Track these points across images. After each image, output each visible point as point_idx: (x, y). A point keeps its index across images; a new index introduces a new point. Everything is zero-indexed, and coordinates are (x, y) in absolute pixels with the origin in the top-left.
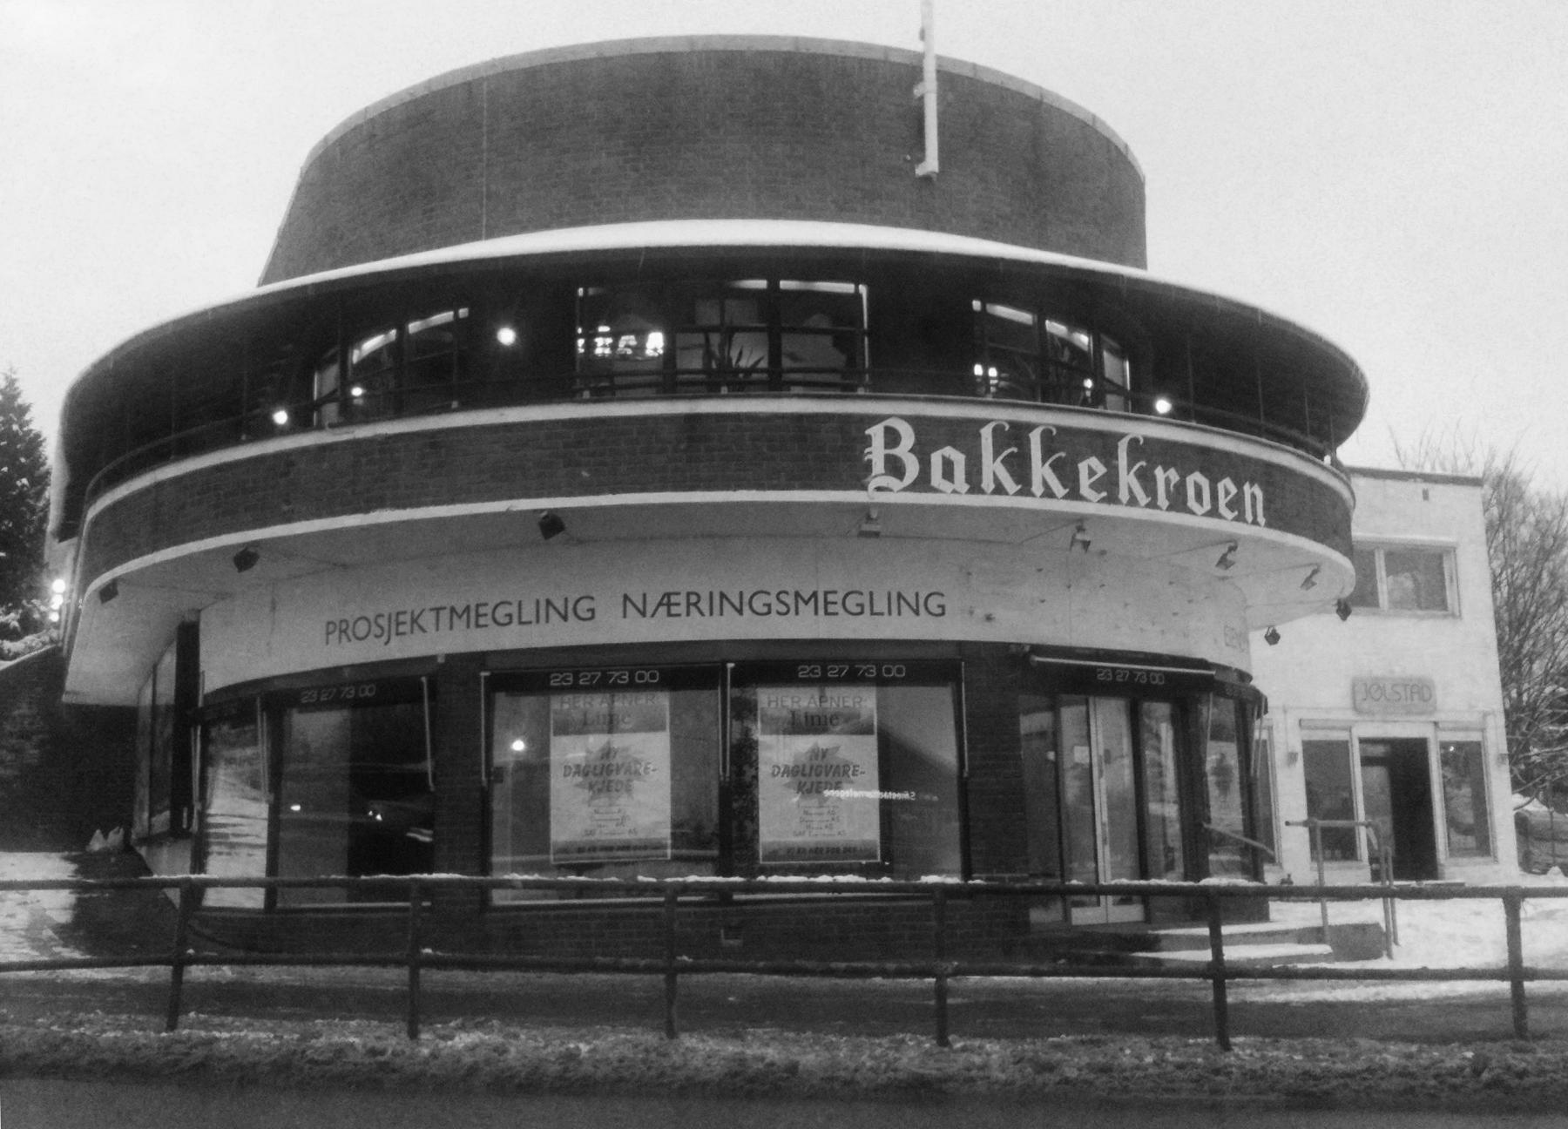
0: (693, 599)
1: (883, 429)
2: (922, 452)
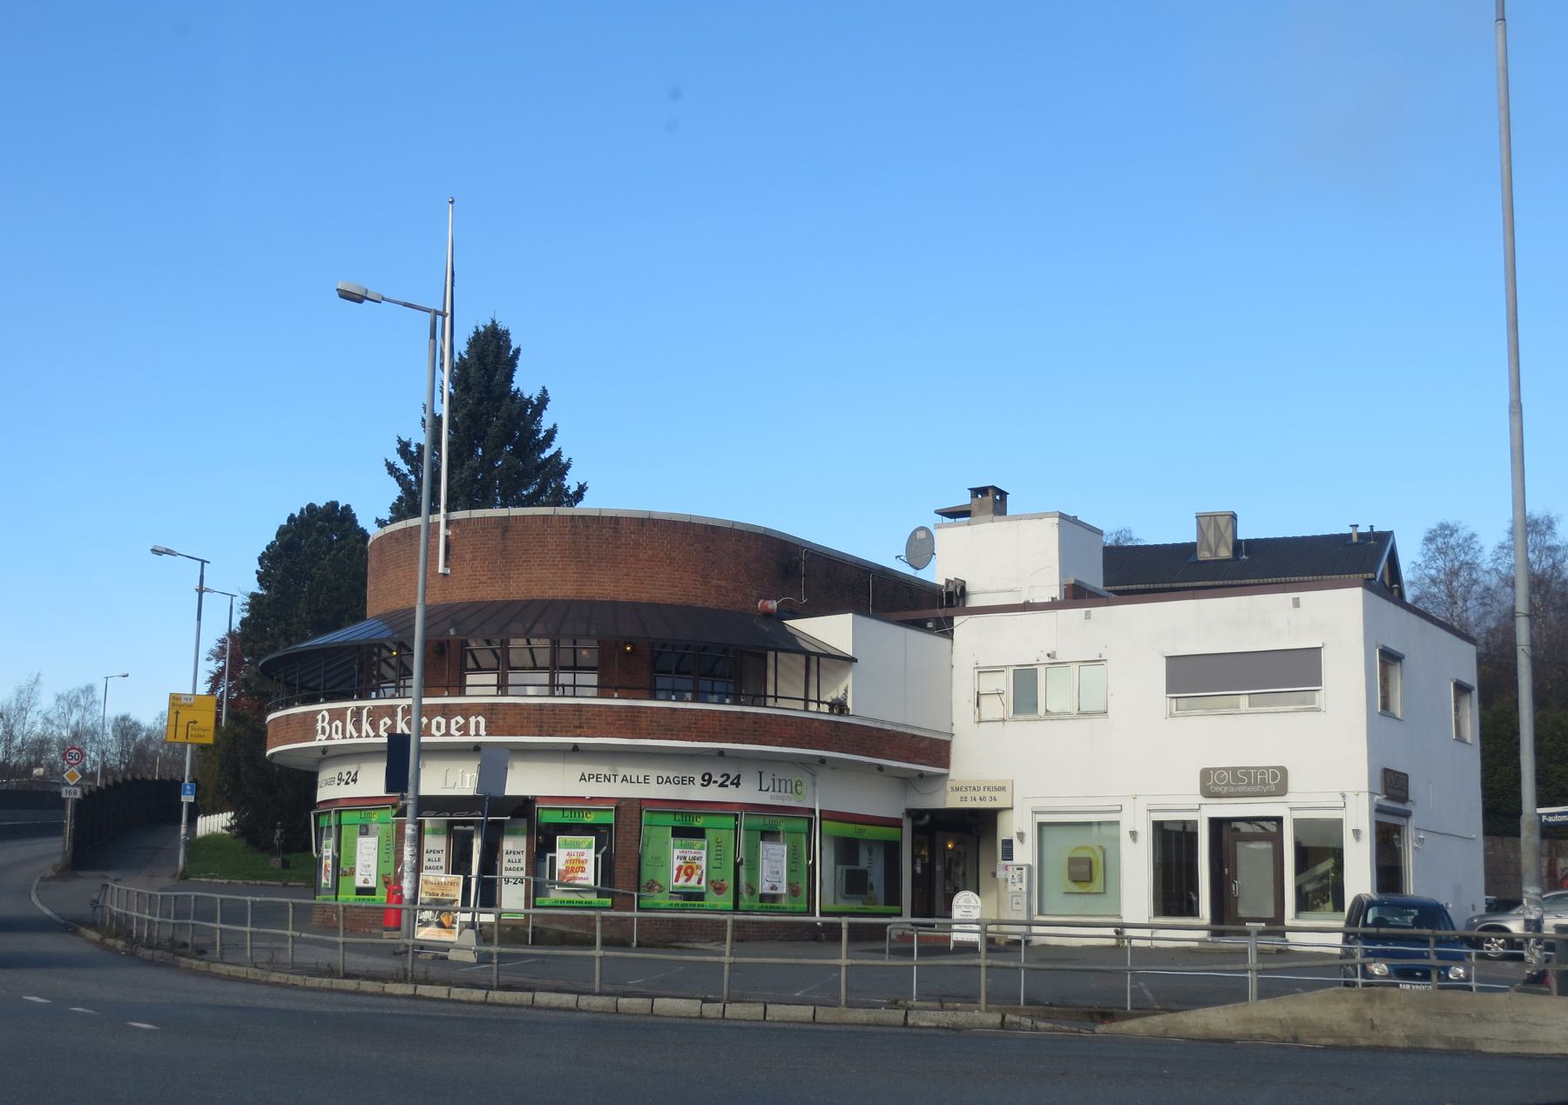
1: (1472, 684)
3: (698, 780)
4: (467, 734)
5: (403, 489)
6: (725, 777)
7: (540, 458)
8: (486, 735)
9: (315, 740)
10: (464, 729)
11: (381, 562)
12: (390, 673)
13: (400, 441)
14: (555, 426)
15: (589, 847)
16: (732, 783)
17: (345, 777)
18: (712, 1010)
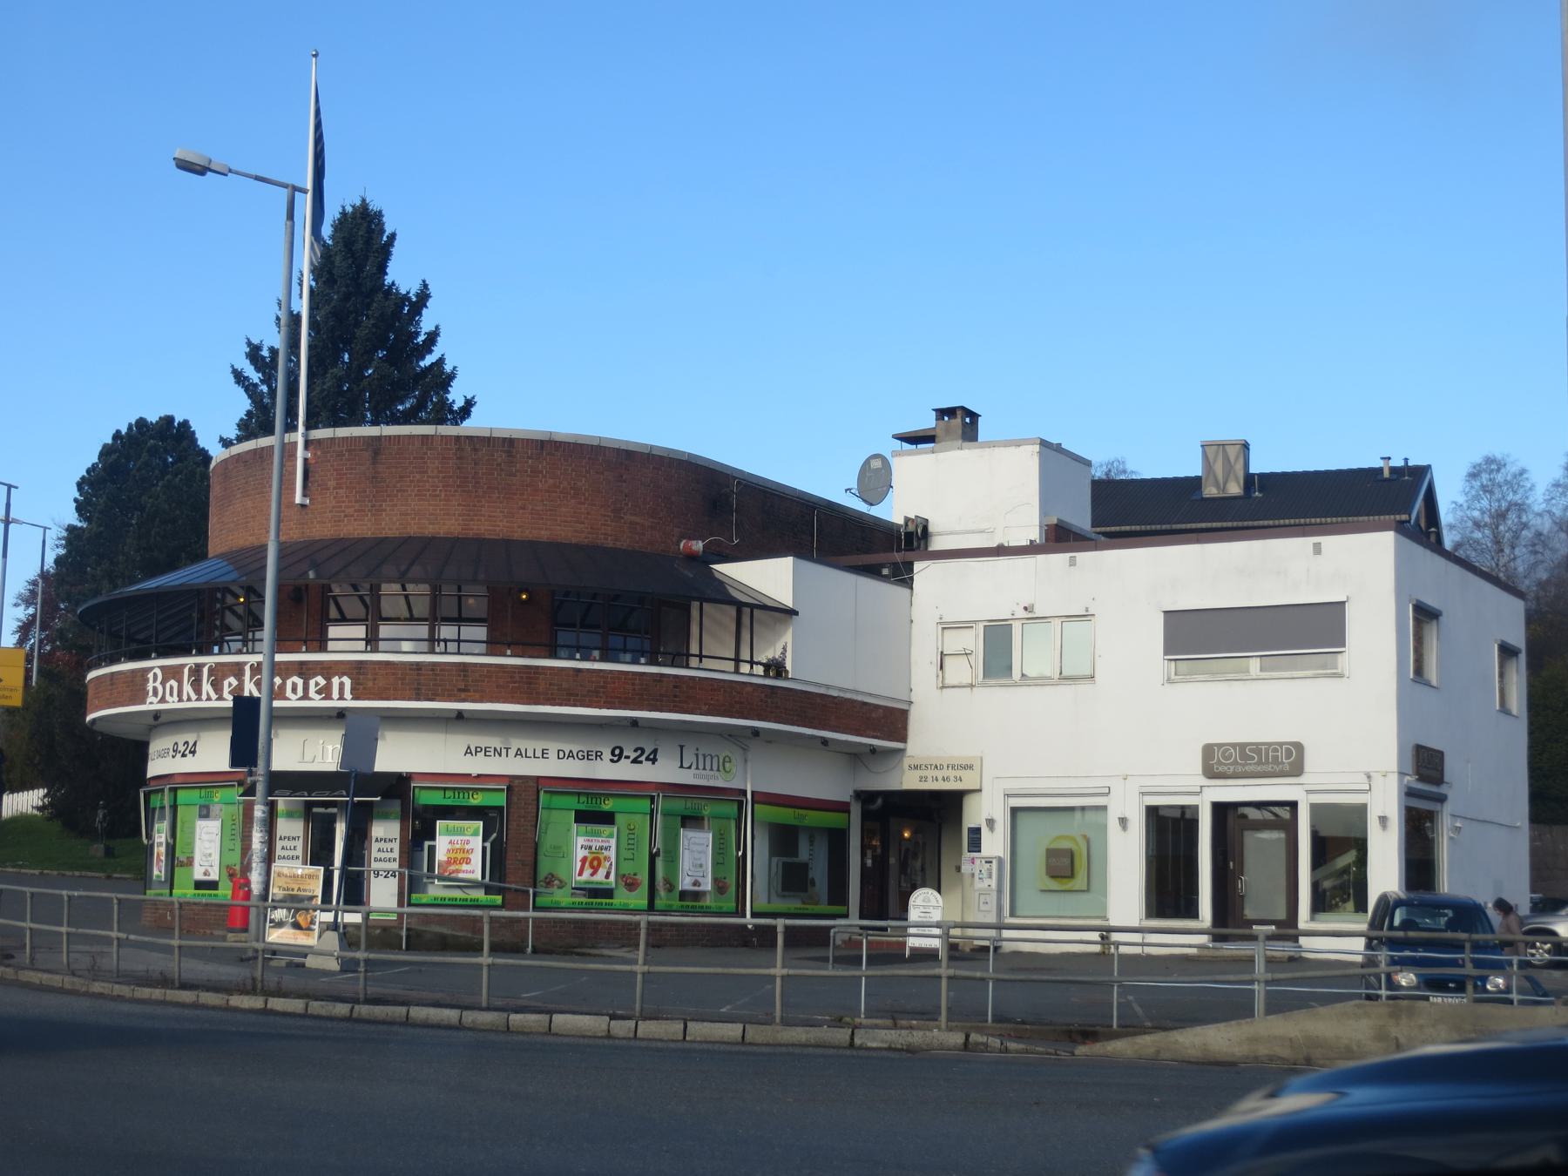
0: (599, 754)
2: (163, 683)
3: (607, 755)
4: (328, 697)
5: (253, 402)
6: (639, 752)
7: (420, 366)
8: (352, 699)
10: (326, 692)
12: (235, 624)
13: (249, 343)
14: (437, 327)
15: (475, 834)
16: (647, 759)
17: (181, 748)
18: (622, 1028)
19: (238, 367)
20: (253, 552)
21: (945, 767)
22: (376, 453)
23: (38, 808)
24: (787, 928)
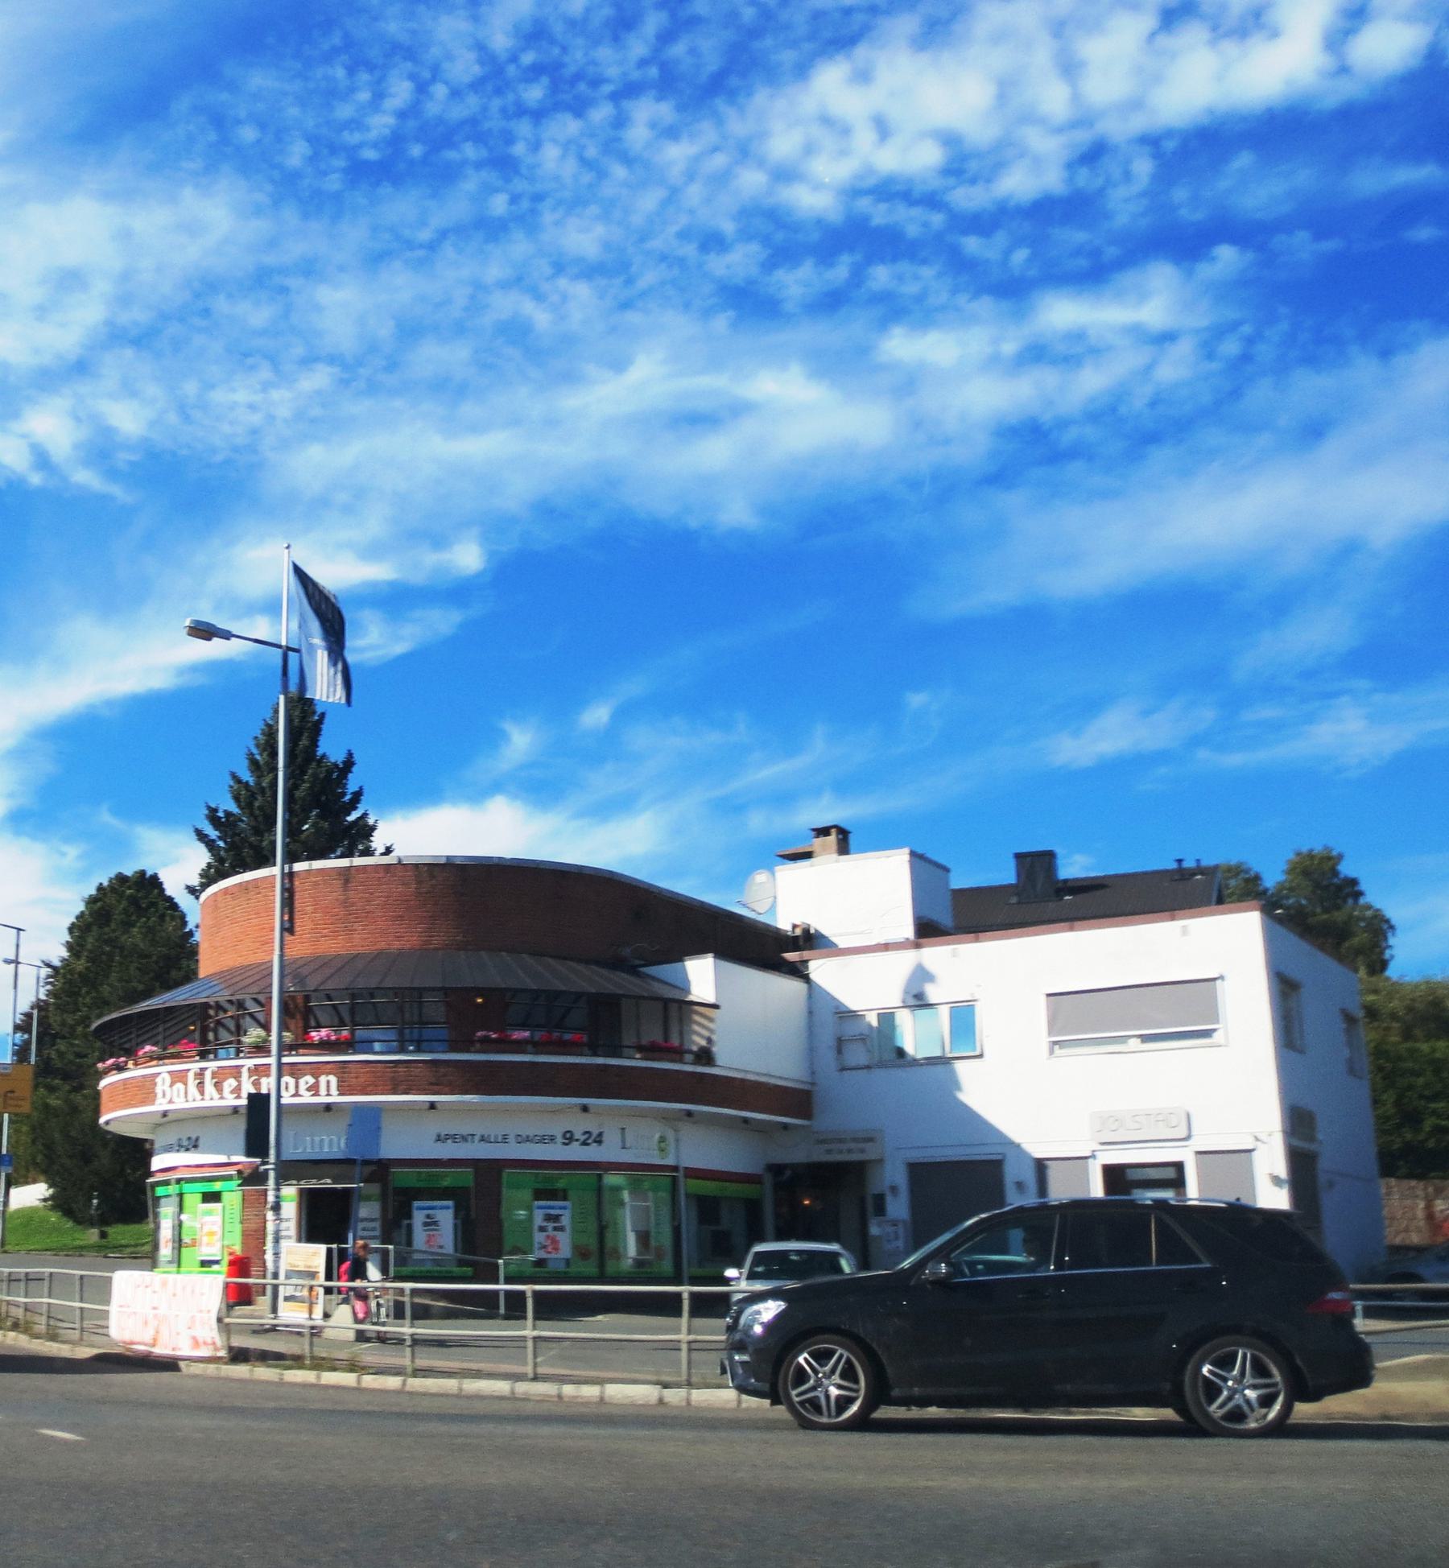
4: (317, 1094)
5: (212, 855)
7: (347, 821)
8: (339, 1095)
9: (153, 1104)
10: (314, 1089)
11: (216, 918)
12: (225, 1036)
13: (209, 808)
14: (361, 788)
16: (595, 1141)
17: (185, 1143)
18: (674, 1396)
19: (200, 827)
20: (257, 970)
21: (512, 1139)
22: (347, 881)
23: (45, 1200)
24: (693, 1295)
